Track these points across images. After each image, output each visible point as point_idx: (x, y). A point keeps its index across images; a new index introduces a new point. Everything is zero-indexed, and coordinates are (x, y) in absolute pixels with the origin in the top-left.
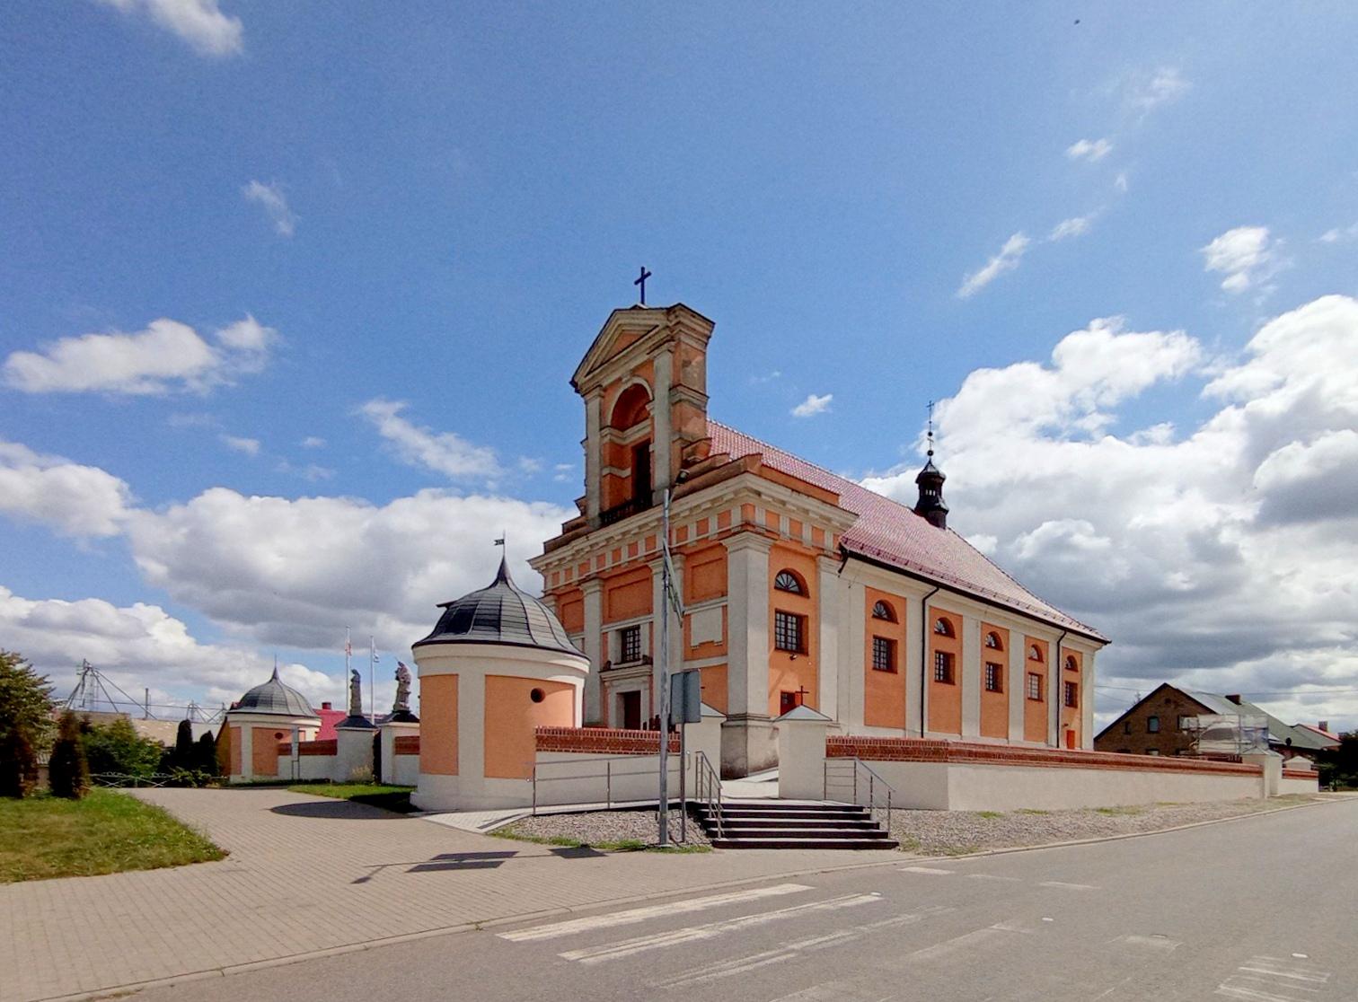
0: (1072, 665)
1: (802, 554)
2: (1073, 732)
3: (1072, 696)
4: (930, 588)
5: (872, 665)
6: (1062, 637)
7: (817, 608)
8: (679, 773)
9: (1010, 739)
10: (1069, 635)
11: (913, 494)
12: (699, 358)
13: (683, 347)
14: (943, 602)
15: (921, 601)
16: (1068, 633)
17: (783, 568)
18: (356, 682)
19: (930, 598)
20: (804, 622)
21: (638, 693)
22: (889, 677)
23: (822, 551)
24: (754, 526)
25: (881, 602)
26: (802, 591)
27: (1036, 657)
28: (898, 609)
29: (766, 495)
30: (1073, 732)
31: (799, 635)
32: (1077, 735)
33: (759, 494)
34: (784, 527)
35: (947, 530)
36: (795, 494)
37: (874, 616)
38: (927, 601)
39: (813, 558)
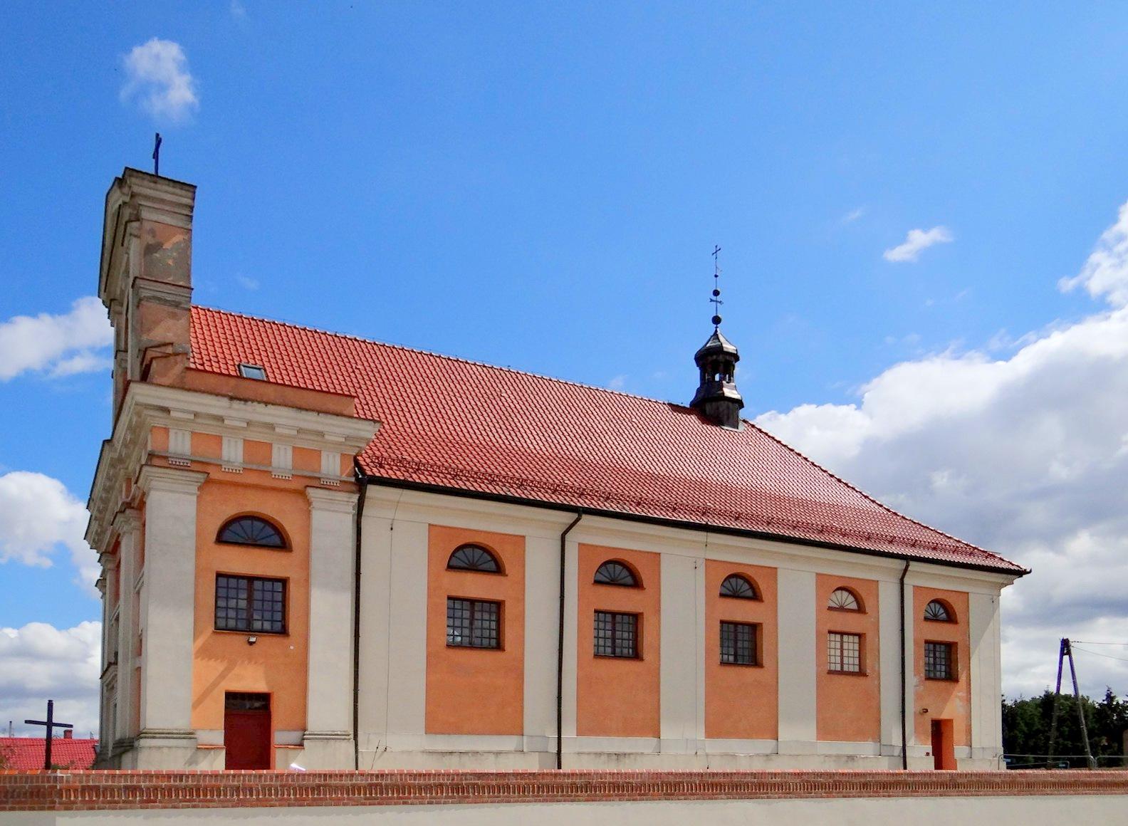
0: (944, 611)
1: (274, 489)
2: (949, 722)
3: (945, 663)
4: (568, 517)
5: (718, 658)
6: (906, 570)
7: (306, 564)
8: (44, 748)
9: (973, 746)
10: (914, 566)
11: (687, 384)
12: (179, 238)
13: (147, 226)
14: (921, 577)
15: (559, 538)
16: (584, 517)
17: (840, 586)
18: (50, 704)
19: (906, 576)
20: (502, 606)
21: (580, 732)
22: (750, 673)
23: (317, 482)
24: (166, 458)
25: (935, 601)
26: (951, 618)
27: (854, 606)
28: (763, 586)
29: (177, 410)
30: (949, 722)
31: (948, 670)
32: (958, 728)
33: (167, 410)
34: (233, 452)
35: (742, 427)
36: (236, 404)
37: (926, 619)
38: (568, 536)
39: (301, 493)
